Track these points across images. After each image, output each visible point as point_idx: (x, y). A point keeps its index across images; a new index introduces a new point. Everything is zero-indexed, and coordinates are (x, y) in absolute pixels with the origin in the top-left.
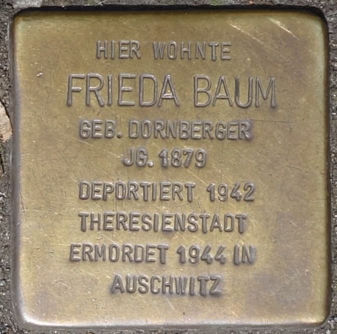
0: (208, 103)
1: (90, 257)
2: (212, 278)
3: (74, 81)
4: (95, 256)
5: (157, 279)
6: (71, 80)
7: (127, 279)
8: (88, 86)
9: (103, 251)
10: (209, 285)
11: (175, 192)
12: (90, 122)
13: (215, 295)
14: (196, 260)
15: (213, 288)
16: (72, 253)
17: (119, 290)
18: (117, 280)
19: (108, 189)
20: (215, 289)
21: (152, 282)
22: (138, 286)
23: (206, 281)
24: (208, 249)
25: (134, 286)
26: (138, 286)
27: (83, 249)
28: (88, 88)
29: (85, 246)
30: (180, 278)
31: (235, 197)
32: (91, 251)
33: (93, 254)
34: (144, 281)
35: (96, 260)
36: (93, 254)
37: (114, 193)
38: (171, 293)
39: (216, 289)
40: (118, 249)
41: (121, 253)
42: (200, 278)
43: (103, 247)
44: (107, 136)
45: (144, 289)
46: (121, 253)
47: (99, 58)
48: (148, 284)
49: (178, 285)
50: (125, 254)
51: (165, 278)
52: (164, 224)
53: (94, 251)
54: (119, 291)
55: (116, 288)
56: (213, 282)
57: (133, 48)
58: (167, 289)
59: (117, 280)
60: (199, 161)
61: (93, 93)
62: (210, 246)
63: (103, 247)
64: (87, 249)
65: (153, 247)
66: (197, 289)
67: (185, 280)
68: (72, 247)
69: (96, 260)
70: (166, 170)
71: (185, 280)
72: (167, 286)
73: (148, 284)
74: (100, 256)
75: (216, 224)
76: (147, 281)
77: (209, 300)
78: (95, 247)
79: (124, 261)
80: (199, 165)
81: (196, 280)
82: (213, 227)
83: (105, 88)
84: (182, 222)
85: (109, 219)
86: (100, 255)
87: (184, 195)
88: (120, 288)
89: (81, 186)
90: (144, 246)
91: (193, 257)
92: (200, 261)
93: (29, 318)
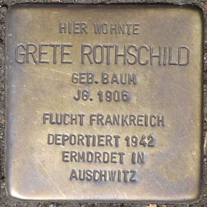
0: (135, 62)
1: (75, 159)
2: (132, 171)
3: (65, 48)
4: (78, 159)
6: (40, 47)
8: (83, 50)
9: (96, 159)
10: (129, 176)
11: (132, 120)
12: (132, 74)
13: (133, 181)
15: (133, 176)
16: (64, 156)
17: (75, 179)
18: (73, 172)
19: (66, 138)
20: (133, 178)
21: (95, 173)
22: (86, 176)
23: (128, 172)
25: (84, 176)
26: (86, 176)
27: (71, 154)
28: (83, 52)
29: (72, 152)
30: (112, 171)
32: (76, 156)
33: (77, 157)
34: (89, 173)
35: (79, 161)
36: (77, 157)
39: (134, 177)
42: (124, 171)
43: (83, 153)
45: (89, 178)
47: (61, 32)
48: (92, 175)
49: (110, 175)
51: (102, 171)
53: (77, 156)
55: (73, 177)
56: (132, 173)
57: (83, 27)
59: (73, 172)
61: (31, 54)
63: (83, 153)
64: (74, 154)
65: (116, 154)
66: (122, 178)
67: (115, 172)
68: (64, 153)
69: (79, 161)
71: (115, 172)
72: (104, 176)
73: (92, 175)
74: (81, 159)
76: (91, 173)
77: (130, 184)
78: (78, 153)
80: (108, 99)
83: (93, 53)
84: (141, 156)
85: (66, 154)
86: (81, 158)
88: (75, 177)
89: (49, 135)
90: (110, 153)
93: (14, 193)
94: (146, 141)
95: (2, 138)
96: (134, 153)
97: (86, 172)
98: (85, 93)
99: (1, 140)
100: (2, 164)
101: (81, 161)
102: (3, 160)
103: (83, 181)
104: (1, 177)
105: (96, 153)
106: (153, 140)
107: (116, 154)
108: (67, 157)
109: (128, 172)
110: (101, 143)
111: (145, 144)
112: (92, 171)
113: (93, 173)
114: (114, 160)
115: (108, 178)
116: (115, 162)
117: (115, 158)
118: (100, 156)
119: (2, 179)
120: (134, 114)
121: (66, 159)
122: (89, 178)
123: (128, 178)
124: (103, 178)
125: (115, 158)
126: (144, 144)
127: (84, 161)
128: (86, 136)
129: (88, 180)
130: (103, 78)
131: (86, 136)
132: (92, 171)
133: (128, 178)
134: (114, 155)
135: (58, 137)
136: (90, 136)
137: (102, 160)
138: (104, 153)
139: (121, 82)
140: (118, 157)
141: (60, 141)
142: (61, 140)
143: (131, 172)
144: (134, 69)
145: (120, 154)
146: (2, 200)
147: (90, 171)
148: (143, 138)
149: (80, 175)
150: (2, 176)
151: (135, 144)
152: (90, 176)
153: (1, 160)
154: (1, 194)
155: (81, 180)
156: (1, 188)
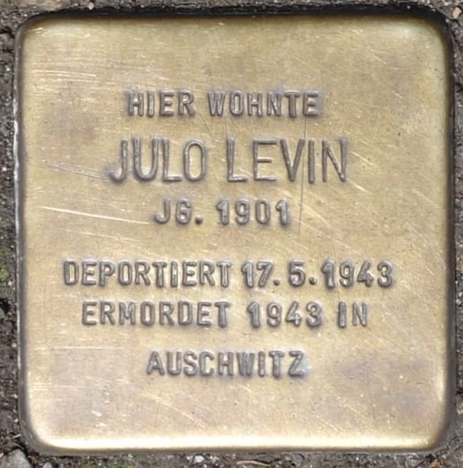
5: (208, 355)
7: (169, 355)
10: (286, 363)
13: (294, 375)
14: (349, 281)
15: (293, 365)
16: (86, 313)
18: (154, 356)
22: (184, 365)
24: (365, 267)
31: (293, 321)
33: (116, 316)
34: (190, 358)
36: (116, 316)
37: (115, 275)
38: (230, 375)
40: (268, 207)
41: (157, 312)
44: (68, 282)
45: (190, 369)
46: (157, 312)
50: (162, 314)
52: (200, 315)
54: (156, 373)
56: (292, 359)
58: (225, 370)
59: (154, 356)
60: (241, 216)
62: (297, 300)
65: (208, 305)
68: (85, 305)
70: (290, 121)
73: (196, 362)
75: (155, 364)
76: (195, 358)
79: (161, 323)
81: (267, 355)
82: (151, 367)
85: (89, 309)
87: (216, 276)
88: (158, 369)
89: (66, 265)
91: (345, 278)
92: (356, 284)
94: (373, 273)
95: (460, 303)
96: (355, 306)
97: (182, 355)
98: (183, 208)
99: (458, 308)
100: (459, 360)
101: (127, 322)
102: (461, 351)
103: (176, 378)
104: (458, 390)
105: (162, 304)
106: (391, 270)
107: (208, 305)
108: (91, 314)
109: (281, 355)
110: (90, 319)
111: (369, 282)
112: (198, 356)
113: (198, 359)
114: (205, 319)
115: (235, 370)
116: (208, 325)
117: (206, 314)
118: (172, 310)
119: (459, 395)
120: (264, 200)
121: (90, 319)
122: (190, 369)
123: (284, 369)
124: (225, 368)
125: (206, 314)
126: (366, 282)
127: (133, 323)
128: (155, 265)
129: (188, 375)
130: (129, 103)
131: (155, 265)
132: (198, 356)
133: (284, 369)
134: (204, 309)
135: (91, 269)
136: (164, 265)
137: (175, 318)
138: (181, 305)
139: (231, 111)
140: (213, 311)
141: (94, 276)
142: (97, 274)
143: (291, 354)
144: (364, 75)
145: (217, 305)
146: (458, 440)
147: (192, 355)
148: (366, 266)
149: (168, 366)
150: (460, 388)
151: (347, 281)
152: (191, 364)
153: (458, 351)
154: (458, 428)
155: (172, 374)
156: (457, 414)
